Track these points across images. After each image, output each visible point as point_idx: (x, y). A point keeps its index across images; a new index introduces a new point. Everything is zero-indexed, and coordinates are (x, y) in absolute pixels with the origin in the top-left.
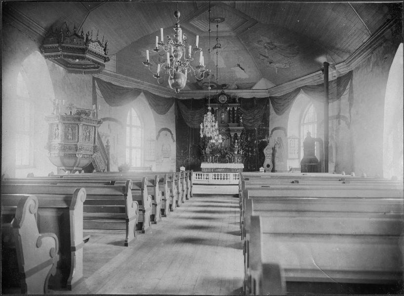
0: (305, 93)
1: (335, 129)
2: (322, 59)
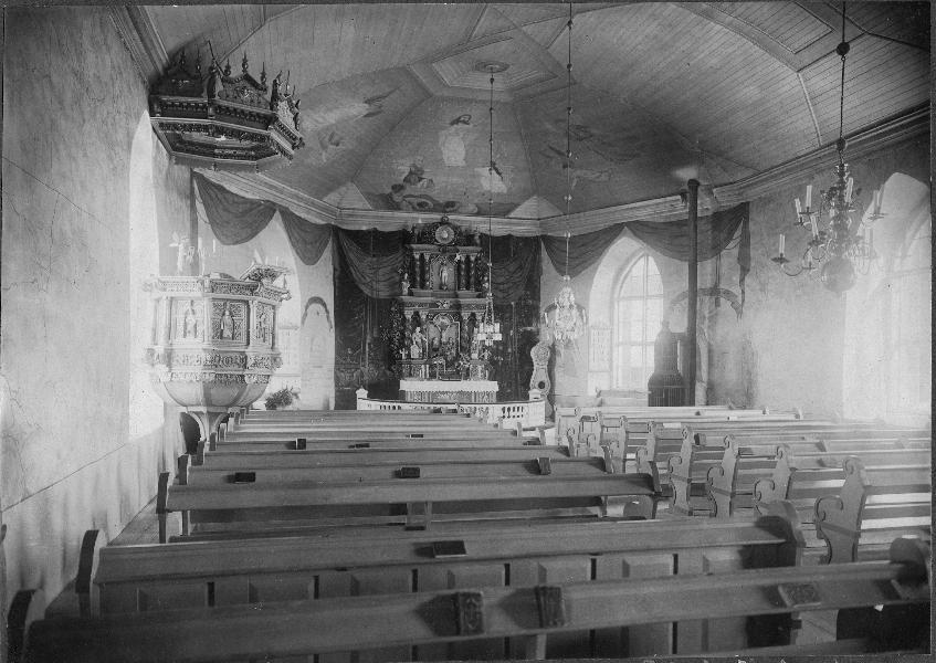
0: (635, 235)
1: (707, 316)
2: (687, 174)
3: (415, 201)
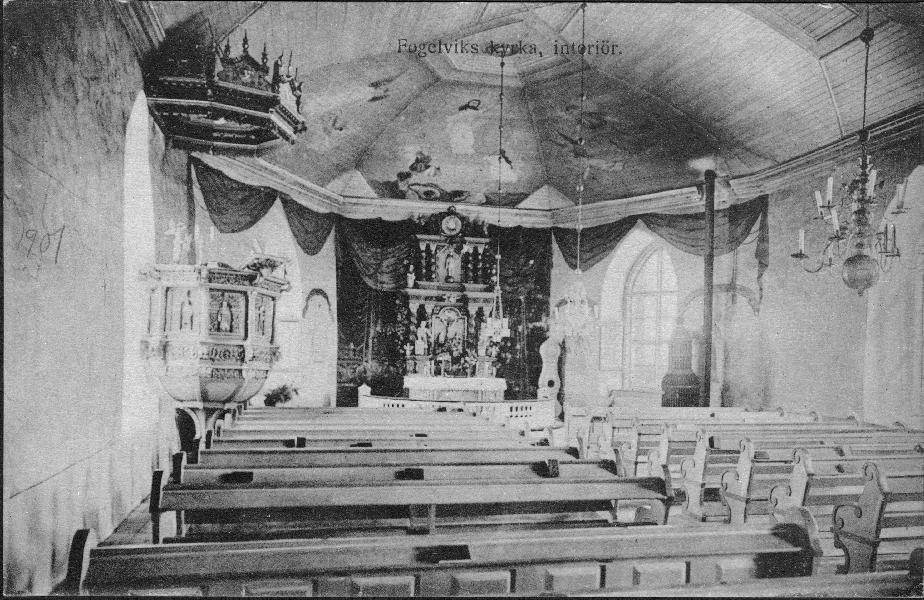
2: (703, 164)
3: (423, 189)
